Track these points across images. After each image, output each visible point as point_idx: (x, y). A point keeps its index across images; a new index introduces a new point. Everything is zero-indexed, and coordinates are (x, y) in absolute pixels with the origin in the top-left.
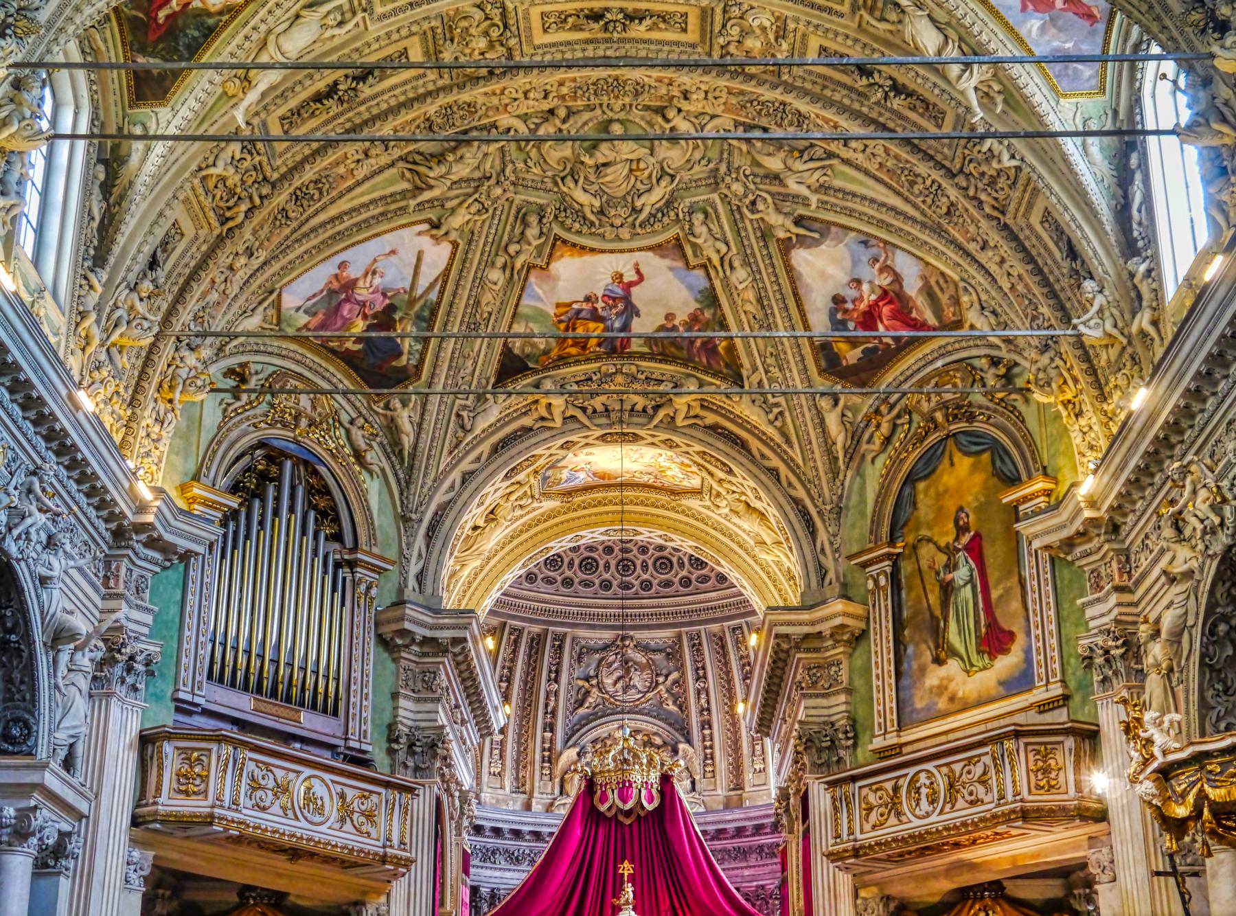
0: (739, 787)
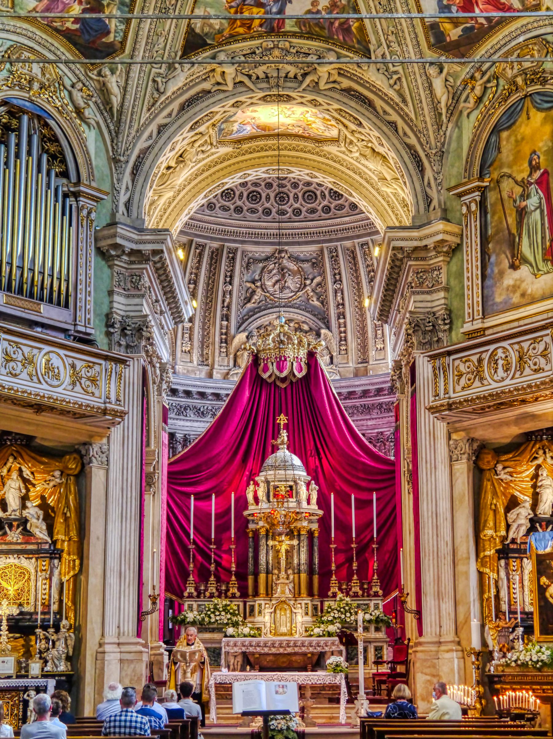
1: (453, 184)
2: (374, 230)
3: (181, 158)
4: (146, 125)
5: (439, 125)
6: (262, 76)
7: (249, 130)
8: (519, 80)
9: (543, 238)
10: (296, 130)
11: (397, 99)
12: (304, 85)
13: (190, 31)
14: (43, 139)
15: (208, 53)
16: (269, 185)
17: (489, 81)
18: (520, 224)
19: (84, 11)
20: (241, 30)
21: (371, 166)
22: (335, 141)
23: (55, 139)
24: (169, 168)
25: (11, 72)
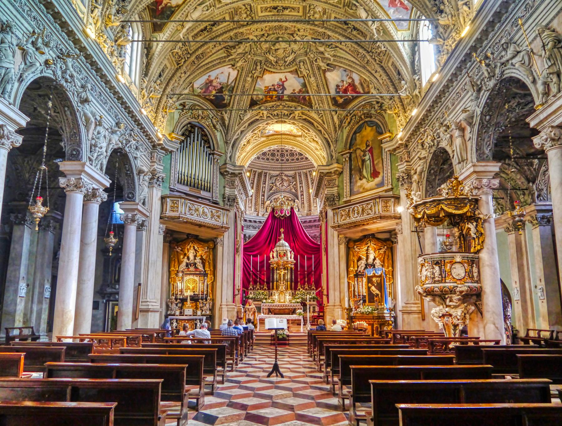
0: (310, 210)
16: (278, 151)
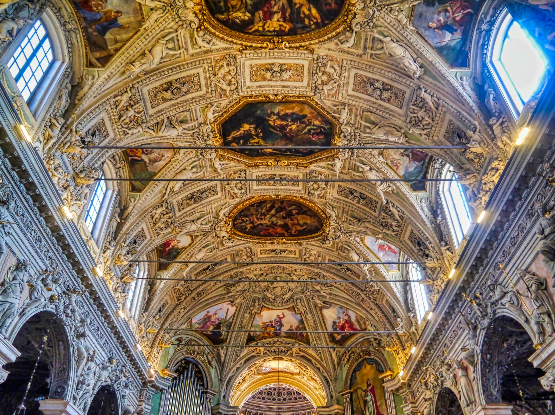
1: (340, 390)
2: (526, 337)
3: (244, 380)
4: (233, 367)
5: (334, 369)
6: (273, 351)
7: (268, 370)
8: (361, 354)
9: (374, 412)
10: (285, 370)
11: (320, 360)
12: (288, 354)
13: (249, 335)
14: (196, 372)
15: (255, 343)
16: (275, 389)
17: (351, 354)
18: (365, 406)
19: (214, 328)
20: (266, 335)
21: (311, 383)
22: (298, 374)
23: (200, 372)
24: (239, 383)
25: (188, 349)
